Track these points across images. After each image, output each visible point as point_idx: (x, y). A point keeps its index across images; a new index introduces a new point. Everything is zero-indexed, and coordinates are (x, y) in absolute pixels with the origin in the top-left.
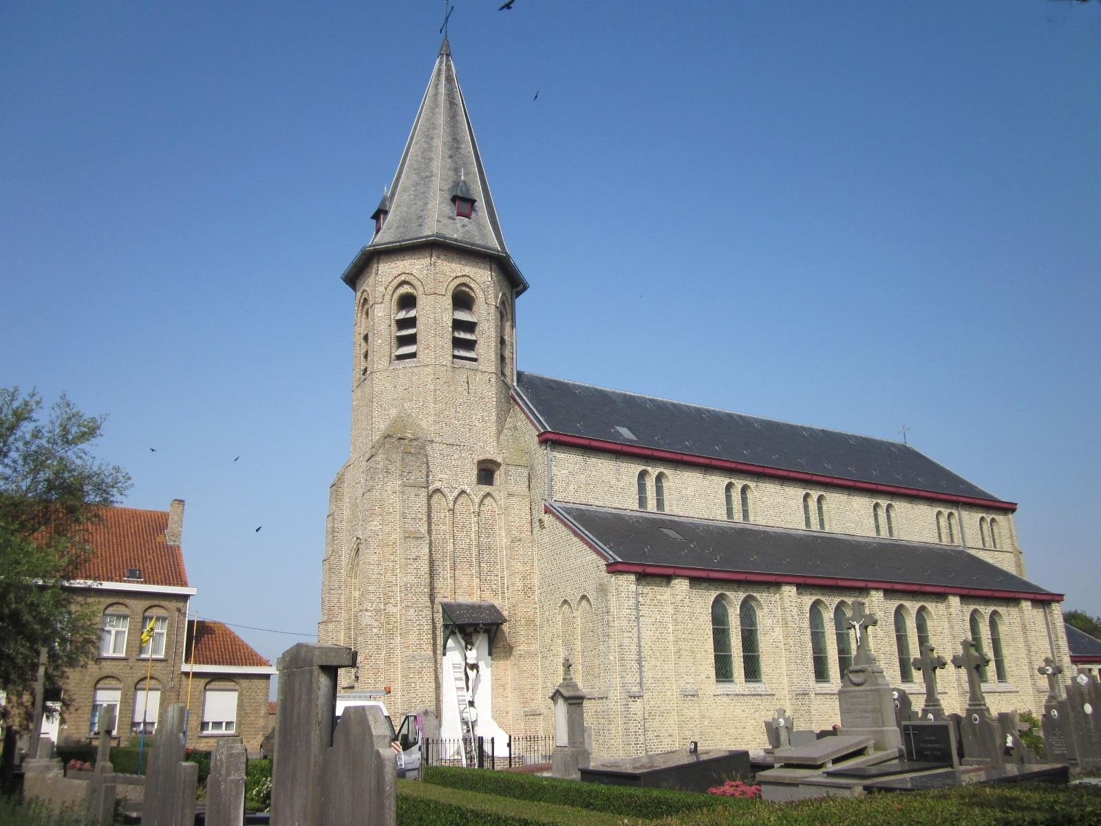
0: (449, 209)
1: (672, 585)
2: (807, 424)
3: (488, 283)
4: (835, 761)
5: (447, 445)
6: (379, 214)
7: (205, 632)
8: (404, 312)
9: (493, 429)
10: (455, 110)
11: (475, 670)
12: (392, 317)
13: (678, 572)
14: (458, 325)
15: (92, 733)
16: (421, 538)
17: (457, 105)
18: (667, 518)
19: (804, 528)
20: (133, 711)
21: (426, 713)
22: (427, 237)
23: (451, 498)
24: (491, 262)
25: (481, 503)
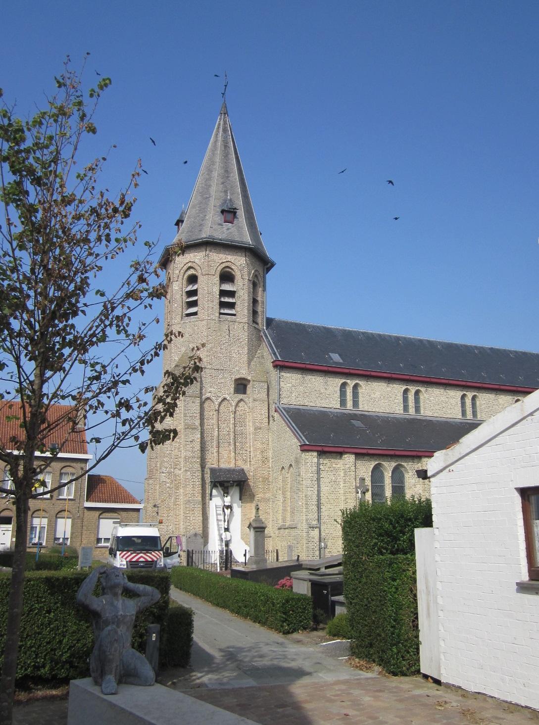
0: (219, 218)
1: (343, 458)
2: (479, 345)
3: (244, 265)
4: (327, 568)
5: (215, 370)
6: (179, 222)
7: (100, 482)
8: (191, 286)
9: (245, 358)
10: (228, 151)
11: (229, 510)
12: (184, 289)
13: (346, 450)
14: (223, 293)
15: (31, 544)
16: (195, 429)
17: (229, 147)
18: (360, 413)
19: (460, 417)
20: (55, 531)
21: (196, 535)
22: (202, 239)
23: (217, 403)
24: (245, 252)
25: (237, 405)
